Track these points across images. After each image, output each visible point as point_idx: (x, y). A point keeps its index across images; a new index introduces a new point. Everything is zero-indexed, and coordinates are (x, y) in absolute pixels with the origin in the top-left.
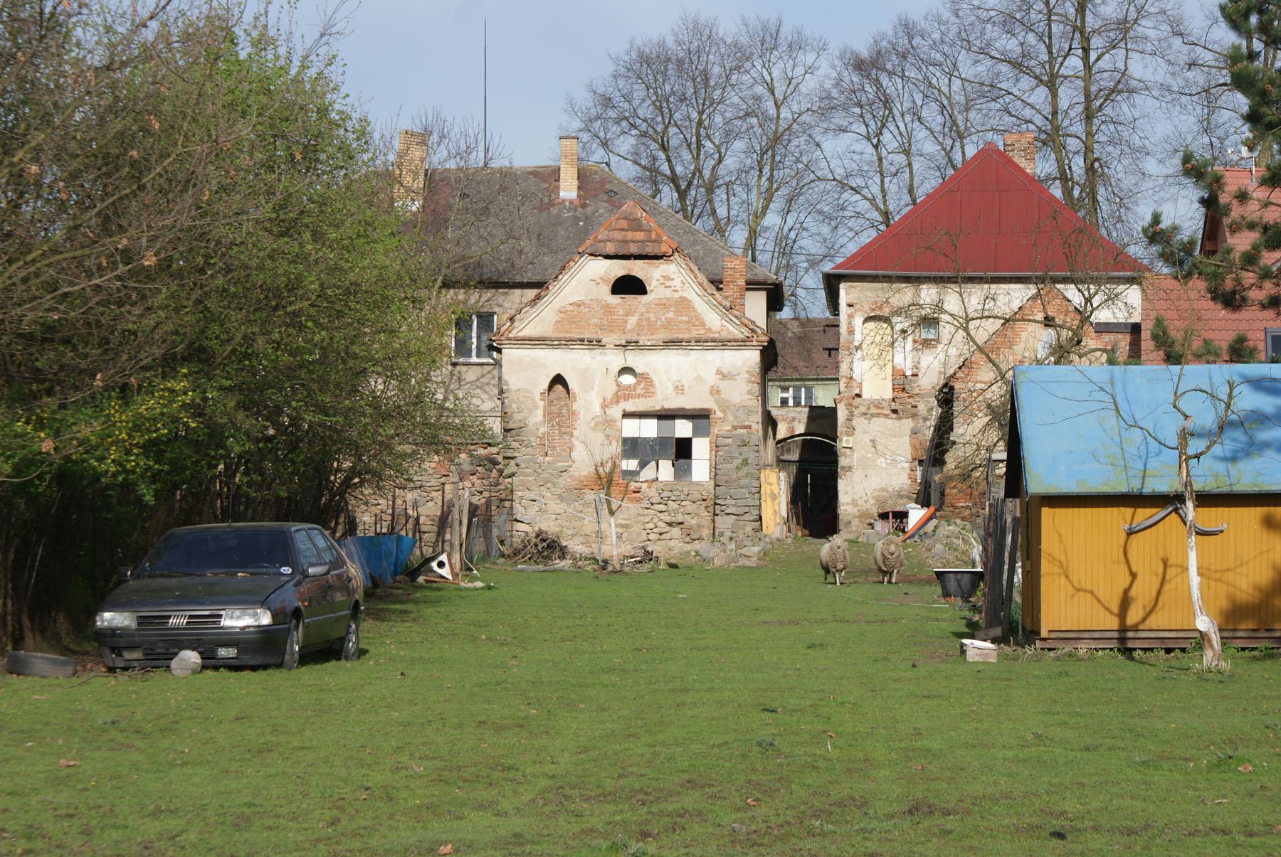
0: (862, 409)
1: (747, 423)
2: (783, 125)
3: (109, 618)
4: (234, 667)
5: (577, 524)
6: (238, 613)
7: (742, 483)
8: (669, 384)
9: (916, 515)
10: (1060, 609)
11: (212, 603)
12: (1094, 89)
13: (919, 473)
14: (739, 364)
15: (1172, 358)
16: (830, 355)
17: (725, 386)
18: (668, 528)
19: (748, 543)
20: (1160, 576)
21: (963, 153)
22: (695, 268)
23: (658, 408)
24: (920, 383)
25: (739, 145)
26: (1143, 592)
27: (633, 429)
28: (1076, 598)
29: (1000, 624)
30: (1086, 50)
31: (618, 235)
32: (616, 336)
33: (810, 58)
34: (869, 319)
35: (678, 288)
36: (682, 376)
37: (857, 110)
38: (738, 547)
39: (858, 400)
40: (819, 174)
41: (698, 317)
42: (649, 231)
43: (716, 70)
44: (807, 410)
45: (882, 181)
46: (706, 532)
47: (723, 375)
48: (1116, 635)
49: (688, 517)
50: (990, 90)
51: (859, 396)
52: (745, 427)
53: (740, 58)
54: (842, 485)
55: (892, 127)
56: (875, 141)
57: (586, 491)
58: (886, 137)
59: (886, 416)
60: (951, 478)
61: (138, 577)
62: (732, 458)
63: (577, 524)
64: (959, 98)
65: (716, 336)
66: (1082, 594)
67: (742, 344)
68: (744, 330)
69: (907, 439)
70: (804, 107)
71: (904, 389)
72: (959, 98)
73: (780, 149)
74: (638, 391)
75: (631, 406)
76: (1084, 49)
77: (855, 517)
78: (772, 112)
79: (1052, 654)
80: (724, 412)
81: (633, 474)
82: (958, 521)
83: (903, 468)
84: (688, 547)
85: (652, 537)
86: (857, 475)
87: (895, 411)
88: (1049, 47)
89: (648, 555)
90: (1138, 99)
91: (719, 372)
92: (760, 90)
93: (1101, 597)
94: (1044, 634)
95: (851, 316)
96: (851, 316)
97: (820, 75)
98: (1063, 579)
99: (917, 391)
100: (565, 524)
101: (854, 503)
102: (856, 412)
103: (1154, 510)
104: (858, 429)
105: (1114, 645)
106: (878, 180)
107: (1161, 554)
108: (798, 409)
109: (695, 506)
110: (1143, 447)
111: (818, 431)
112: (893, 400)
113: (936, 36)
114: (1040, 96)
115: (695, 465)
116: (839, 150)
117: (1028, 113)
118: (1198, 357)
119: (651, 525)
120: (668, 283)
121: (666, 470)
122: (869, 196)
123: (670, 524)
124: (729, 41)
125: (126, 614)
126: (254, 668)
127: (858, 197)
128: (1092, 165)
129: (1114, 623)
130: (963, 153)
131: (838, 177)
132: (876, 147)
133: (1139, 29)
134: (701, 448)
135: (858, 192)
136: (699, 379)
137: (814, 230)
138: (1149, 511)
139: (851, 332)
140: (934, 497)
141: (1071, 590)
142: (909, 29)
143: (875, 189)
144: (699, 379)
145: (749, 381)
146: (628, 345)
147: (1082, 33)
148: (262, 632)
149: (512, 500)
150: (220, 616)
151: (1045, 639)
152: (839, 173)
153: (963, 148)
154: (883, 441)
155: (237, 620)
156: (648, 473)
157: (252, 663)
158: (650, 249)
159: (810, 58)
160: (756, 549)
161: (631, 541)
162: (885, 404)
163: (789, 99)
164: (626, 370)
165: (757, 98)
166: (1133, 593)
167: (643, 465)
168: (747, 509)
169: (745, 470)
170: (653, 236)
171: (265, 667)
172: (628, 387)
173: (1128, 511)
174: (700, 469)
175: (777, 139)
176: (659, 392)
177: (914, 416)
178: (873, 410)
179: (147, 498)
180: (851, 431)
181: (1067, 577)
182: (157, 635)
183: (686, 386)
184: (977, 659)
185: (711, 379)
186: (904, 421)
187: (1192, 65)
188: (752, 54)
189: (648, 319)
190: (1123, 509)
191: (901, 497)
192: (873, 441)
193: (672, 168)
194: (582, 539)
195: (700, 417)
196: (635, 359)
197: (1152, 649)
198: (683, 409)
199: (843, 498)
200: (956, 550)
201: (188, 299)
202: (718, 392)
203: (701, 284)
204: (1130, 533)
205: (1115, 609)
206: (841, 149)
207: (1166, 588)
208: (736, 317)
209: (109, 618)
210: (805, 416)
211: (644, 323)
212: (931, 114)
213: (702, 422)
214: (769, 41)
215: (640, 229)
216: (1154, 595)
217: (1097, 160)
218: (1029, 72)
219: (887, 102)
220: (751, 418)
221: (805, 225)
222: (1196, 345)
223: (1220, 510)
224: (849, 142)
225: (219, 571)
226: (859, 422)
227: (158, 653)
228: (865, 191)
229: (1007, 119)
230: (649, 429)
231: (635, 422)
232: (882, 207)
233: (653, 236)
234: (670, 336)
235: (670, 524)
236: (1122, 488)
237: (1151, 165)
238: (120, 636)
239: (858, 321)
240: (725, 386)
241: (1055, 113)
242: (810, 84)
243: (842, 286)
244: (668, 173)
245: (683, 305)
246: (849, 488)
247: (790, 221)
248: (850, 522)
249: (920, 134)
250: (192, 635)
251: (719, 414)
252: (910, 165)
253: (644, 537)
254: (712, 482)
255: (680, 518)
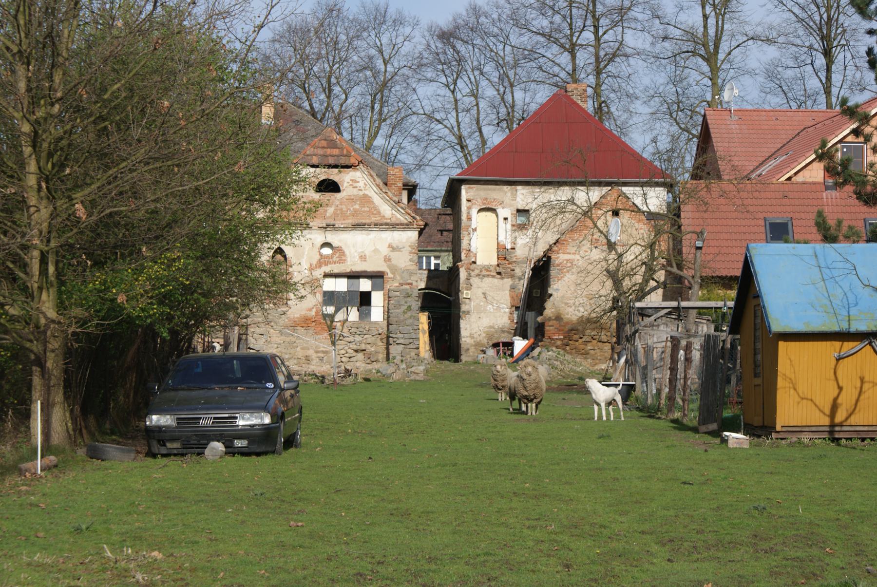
0: (477, 272)
1: (409, 281)
3: (155, 419)
4: (244, 453)
5: (292, 351)
6: (248, 415)
7: (408, 322)
9: (520, 345)
10: (789, 411)
11: (230, 409)
12: (602, 53)
13: (515, 316)
14: (404, 241)
15: (829, 238)
17: (394, 255)
18: (354, 354)
20: (859, 389)
22: (374, 175)
23: (348, 270)
25: (357, 90)
26: (846, 400)
27: (330, 285)
28: (800, 405)
29: (715, 421)
30: (596, 28)
31: (320, 152)
33: (408, 30)
34: (481, 210)
36: (364, 248)
37: (440, 67)
38: (408, 367)
39: (474, 265)
40: (414, 109)
41: (375, 208)
42: (342, 148)
43: (343, 37)
44: (426, 272)
45: (457, 115)
46: (382, 356)
48: (827, 429)
49: (368, 346)
50: (531, 54)
51: (474, 263)
52: (409, 284)
53: (360, 29)
54: (463, 324)
56: (452, 87)
57: (298, 328)
58: (460, 84)
59: (493, 276)
60: (550, 319)
61: (165, 390)
62: (400, 305)
63: (292, 351)
64: (509, 59)
65: (388, 221)
66: (805, 401)
67: (406, 227)
68: (408, 217)
69: (507, 292)
70: (402, 64)
71: (505, 258)
72: (509, 59)
74: (335, 259)
75: (327, 269)
76: (594, 26)
77: (472, 345)
79: (783, 442)
80: (393, 273)
82: (554, 349)
83: (505, 312)
84: (370, 367)
85: (344, 359)
86: (473, 317)
87: (499, 273)
88: (570, 25)
89: (348, 372)
90: (632, 61)
91: (390, 246)
92: (373, 52)
93: (817, 403)
94: (778, 428)
95: (469, 208)
96: (469, 208)
97: (415, 43)
98: (792, 391)
99: (514, 259)
101: (471, 336)
102: (473, 274)
103: (855, 343)
104: (474, 285)
105: (826, 435)
106: (455, 115)
107: (859, 375)
109: (373, 338)
110: (845, 300)
111: (434, 287)
112: (498, 265)
113: (495, 16)
114: (565, 59)
117: (556, 69)
118: (847, 238)
120: (355, 185)
121: (354, 315)
122: (449, 125)
123: (356, 351)
124: (351, 18)
125: (168, 417)
126: (258, 454)
127: (440, 126)
129: (826, 421)
132: (453, 92)
133: (633, 13)
134: (377, 298)
135: (441, 123)
136: (376, 251)
137: (409, 148)
138: (851, 344)
139: (469, 219)
140: (531, 332)
141: (797, 399)
142: (476, 11)
143: (453, 121)
145: (411, 253)
146: (329, 227)
147: (594, 16)
148: (265, 429)
149: (247, 335)
150: (236, 418)
151: (778, 432)
152: (428, 109)
154: (491, 294)
155: (245, 420)
156: (340, 316)
157: (258, 451)
158: (343, 161)
159: (408, 30)
160: (422, 368)
161: (329, 363)
162: (492, 268)
165: (371, 58)
166: (839, 401)
167: (337, 311)
168: (411, 341)
169: (409, 314)
170: (345, 152)
171: (265, 453)
172: (327, 256)
173: (837, 344)
174: (377, 313)
175: (385, 84)
176: (349, 259)
177: (512, 276)
178: (484, 273)
179: (165, 335)
180: (469, 286)
181: (795, 389)
182: (192, 431)
184: (735, 446)
185: (385, 251)
186: (506, 280)
187: (665, 38)
188: (368, 27)
189: (341, 209)
190: (834, 343)
191: (503, 332)
192: (484, 294)
193: (311, 105)
195: (377, 277)
196: (333, 238)
197: (851, 439)
198: (365, 272)
199: (463, 333)
200: (556, 368)
202: (389, 260)
203: (378, 186)
204: (838, 359)
205: (827, 411)
206: (429, 93)
207: (862, 397)
208: (402, 208)
209: (155, 419)
210: (425, 276)
213: (379, 280)
214: (379, 19)
215: (336, 147)
216: (854, 402)
217: (603, 102)
218: (556, 41)
219: (460, 61)
222: (844, 229)
223: (806, 343)
226: (475, 281)
227: (192, 443)
228: (445, 122)
229: (541, 74)
230: (341, 285)
233: (345, 152)
234: (356, 221)
235: (356, 351)
236: (836, 328)
238: (165, 432)
239: (474, 211)
240: (394, 255)
241: (574, 70)
242: (407, 48)
243: (463, 187)
244: (308, 108)
247: (392, 143)
248: (468, 349)
249: (484, 83)
250: (217, 431)
252: (477, 105)
253: (338, 359)
254: (385, 322)
255: (363, 347)
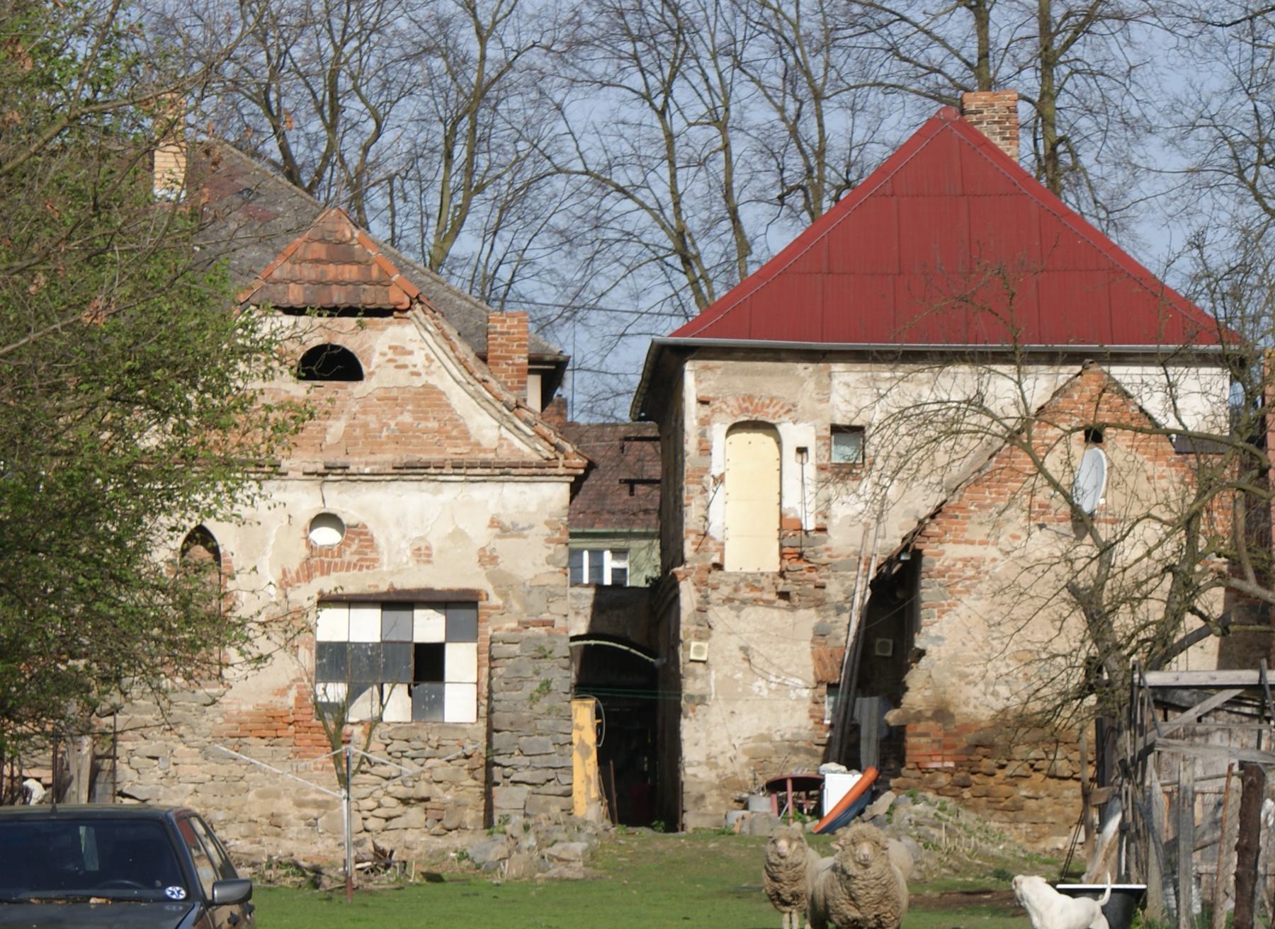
0: (725, 591)
1: (546, 616)
2: (490, 71)
5: (235, 802)
8: (404, 545)
13: (827, 708)
16: (632, 492)
18: (400, 809)
19: (560, 836)
21: (821, 125)
23: (384, 587)
24: (829, 543)
25: (407, 108)
27: (337, 626)
31: (309, 272)
32: (306, 456)
34: (735, 428)
35: (420, 369)
38: (542, 844)
39: (716, 574)
40: (558, 160)
41: (456, 422)
42: (366, 264)
44: (591, 592)
45: (673, 176)
46: (472, 815)
47: (502, 529)
49: (438, 789)
51: (719, 566)
52: (544, 624)
54: (689, 729)
55: (696, 79)
56: (659, 102)
57: (252, 740)
58: (681, 92)
59: (769, 604)
60: (919, 717)
62: (522, 680)
63: (235, 802)
65: (490, 456)
69: (806, 646)
70: (527, 39)
71: (801, 556)
73: (484, 115)
74: (348, 557)
75: (328, 584)
77: (712, 787)
78: (474, 49)
80: (504, 595)
81: (340, 710)
82: (930, 795)
83: (799, 699)
84: (440, 843)
85: (371, 824)
86: (716, 711)
87: (784, 595)
89: (382, 858)
91: (494, 523)
95: (705, 422)
96: (705, 422)
99: (824, 558)
100: (212, 801)
101: (711, 762)
102: (714, 596)
104: (719, 628)
108: (577, 590)
109: (450, 767)
112: (781, 574)
115: (450, 691)
116: (597, 118)
119: (370, 803)
121: (398, 704)
122: (650, 203)
123: (405, 801)
127: (628, 204)
128: (1054, 148)
130: (821, 125)
131: (591, 168)
132: (662, 114)
134: (461, 662)
135: (629, 196)
136: (458, 535)
137: (544, 262)
140: (868, 750)
143: (661, 190)
145: (549, 540)
149: (115, 758)
152: (596, 159)
153: (820, 117)
154: (763, 649)
156: (361, 710)
158: (369, 297)
160: (579, 847)
161: (334, 832)
162: (765, 582)
163: (499, 27)
164: (326, 519)
165: (443, 24)
167: (353, 695)
168: (551, 774)
169: (545, 703)
170: (375, 273)
172: (327, 550)
174: (460, 701)
175: (480, 94)
176: (385, 559)
177: (819, 604)
178: (745, 593)
180: (706, 629)
183: (435, 546)
185: (481, 535)
186: (802, 613)
189: (365, 426)
192: (744, 649)
193: (284, 149)
194: (243, 829)
195: (459, 605)
196: (339, 499)
198: (430, 591)
200: (936, 847)
202: (493, 559)
203: (462, 362)
208: (526, 422)
211: (358, 432)
212: (757, 51)
213: (464, 614)
217: (1062, 140)
220: (553, 608)
221: (527, 255)
224: (614, 104)
225: (53, 894)
226: (720, 615)
228: (642, 194)
229: (895, 65)
232: (674, 222)
235: (405, 801)
237: (1154, 151)
239: (718, 431)
240: (505, 547)
241: (984, 56)
244: (277, 156)
245: (430, 398)
246: (702, 735)
247: (500, 248)
248: (702, 797)
251: (495, 600)
252: (726, 147)
253: (358, 824)
254: (482, 724)
255: (423, 790)
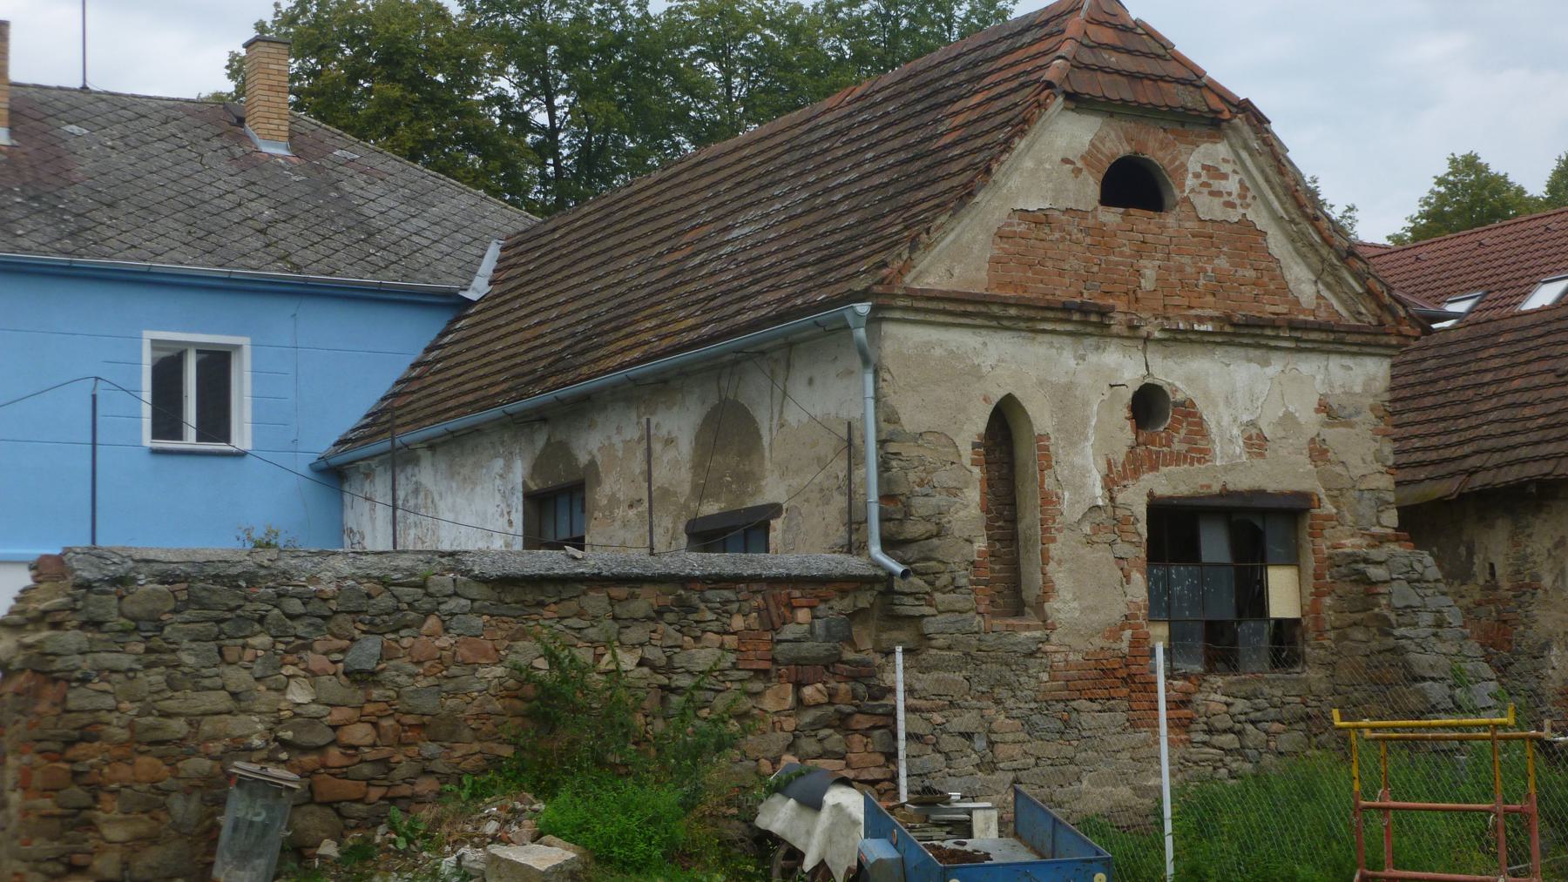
91: (1324, 407)
136: (1288, 420)
144: (1288, 420)
201: (1554, 730)
231: (1087, 75)
